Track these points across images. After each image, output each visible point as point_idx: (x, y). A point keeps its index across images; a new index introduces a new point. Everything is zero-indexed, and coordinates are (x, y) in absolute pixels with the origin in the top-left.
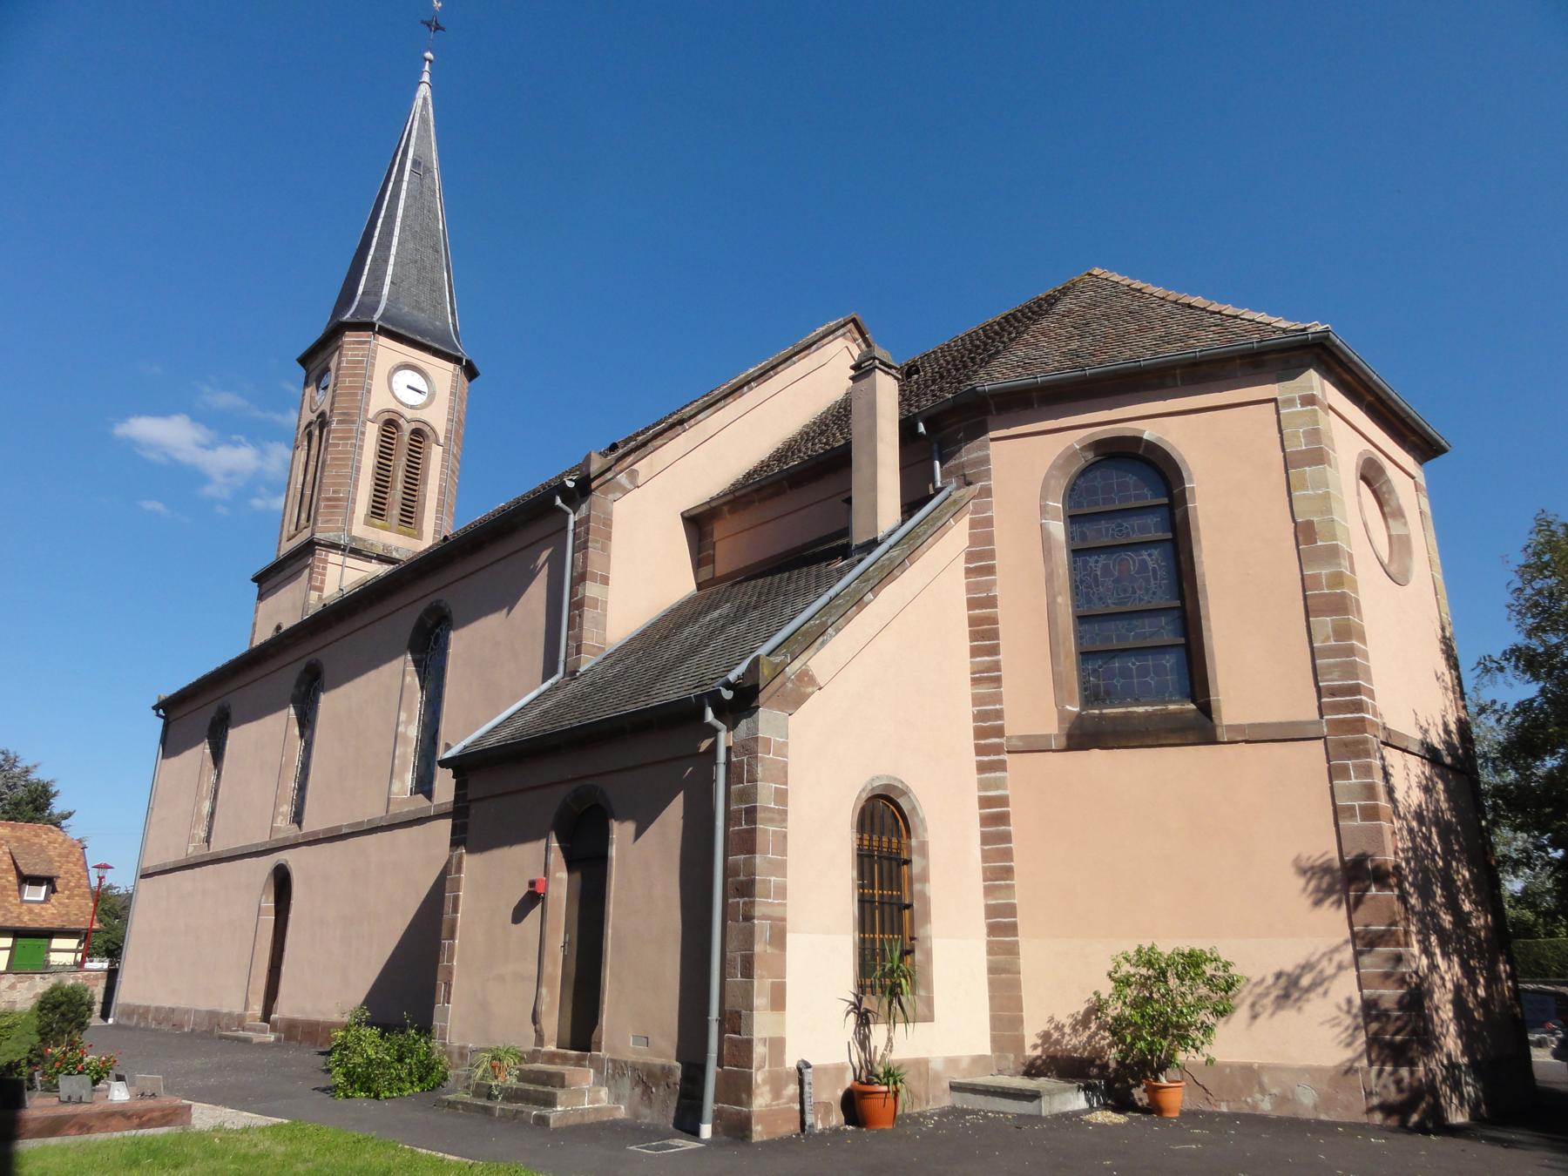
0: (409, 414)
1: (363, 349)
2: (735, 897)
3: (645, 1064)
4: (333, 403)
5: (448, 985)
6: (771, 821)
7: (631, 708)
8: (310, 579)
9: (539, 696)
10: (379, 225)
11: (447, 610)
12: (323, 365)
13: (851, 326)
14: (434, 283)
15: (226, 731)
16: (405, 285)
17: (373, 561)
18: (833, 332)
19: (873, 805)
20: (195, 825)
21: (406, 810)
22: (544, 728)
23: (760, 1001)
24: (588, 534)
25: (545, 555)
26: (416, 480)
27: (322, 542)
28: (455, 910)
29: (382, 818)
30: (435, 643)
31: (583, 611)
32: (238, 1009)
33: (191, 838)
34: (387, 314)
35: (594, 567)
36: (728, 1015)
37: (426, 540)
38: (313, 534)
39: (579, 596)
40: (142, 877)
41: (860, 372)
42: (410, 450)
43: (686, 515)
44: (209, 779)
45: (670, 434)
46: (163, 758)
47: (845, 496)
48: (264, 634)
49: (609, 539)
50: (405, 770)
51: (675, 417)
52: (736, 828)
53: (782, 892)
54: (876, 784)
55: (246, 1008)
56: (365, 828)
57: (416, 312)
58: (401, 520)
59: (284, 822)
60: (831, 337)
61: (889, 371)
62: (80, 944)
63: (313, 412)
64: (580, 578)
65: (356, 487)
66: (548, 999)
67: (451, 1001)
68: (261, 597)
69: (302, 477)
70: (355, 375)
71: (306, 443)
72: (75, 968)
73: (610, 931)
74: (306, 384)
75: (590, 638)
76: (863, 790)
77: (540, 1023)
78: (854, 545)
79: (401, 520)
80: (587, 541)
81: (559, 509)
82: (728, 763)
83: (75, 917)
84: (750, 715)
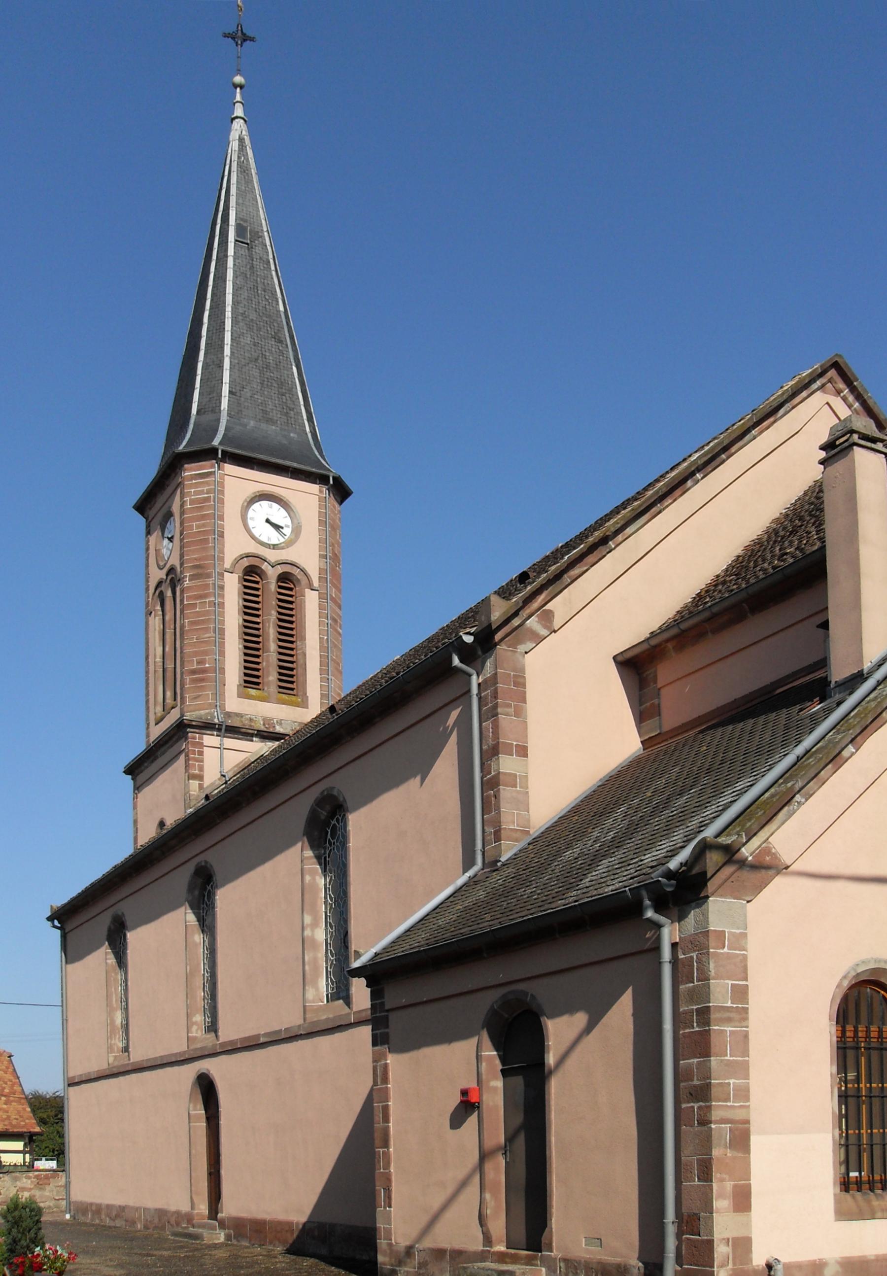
0: (273, 556)
1: (207, 483)
2: (689, 1102)
3: (600, 1263)
4: (182, 556)
5: (388, 1191)
6: (729, 1020)
7: (560, 905)
8: (187, 766)
9: (455, 893)
10: (206, 319)
11: (341, 799)
12: (164, 510)
13: (832, 373)
14: (281, 384)
15: (125, 936)
16: (247, 393)
17: (254, 739)
18: (806, 386)
19: (859, 993)
20: (111, 1035)
21: (324, 1017)
22: (462, 931)
23: (721, 1204)
24: (496, 698)
25: (454, 714)
26: (292, 636)
27: (194, 723)
28: (386, 1119)
29: (299, 1026)
30: (333, 837)
31: (499, 790)
32: (185, 1208)
33: (110, 1049)
34: (230, 434)
35: (508, 734)
36: (685, 1218)
37: (313, 709)
38: (182, 715)
39: (493, 773)
40: (69, 1085)
41: (833, 452)
42: (280, 600)
43: (620, 659)
44: (116, 989)
45: (590, 559)
46: (66, 963)
47: (819, 620)
48: (148, 834)
49: (524, 701)
50: (317, 977)
51: (597, 534)
52: (687, 1031)
53: (744, 1094)
54: (861, 969)
55: (193, 1207)
56: (283, 1037)
57: (264, 426)
58: (280, 687)
59: (199, 1032)
60: (804, 394)
61: (873, 446)
62: (25, 1145)
63: (161, 569)
64: (492, 752)
65: (222, 653)
66: (493, 1203)
67: (393, 1205)
68: (137, 788)
69: (161, 648)
70: (203, 517)
71: (159, 608)
72: (25, 1169)
73: (553, 1139)
74: (149, 533)
75: (510, 819)
76: (845, 977)
77: (486, 1225)
78: (833, 682)
79: (280, 687)
80: (496, 706)
81: (457, 670)
82: (675, 961)
83: (16, 1121)
84: (699, 906)
